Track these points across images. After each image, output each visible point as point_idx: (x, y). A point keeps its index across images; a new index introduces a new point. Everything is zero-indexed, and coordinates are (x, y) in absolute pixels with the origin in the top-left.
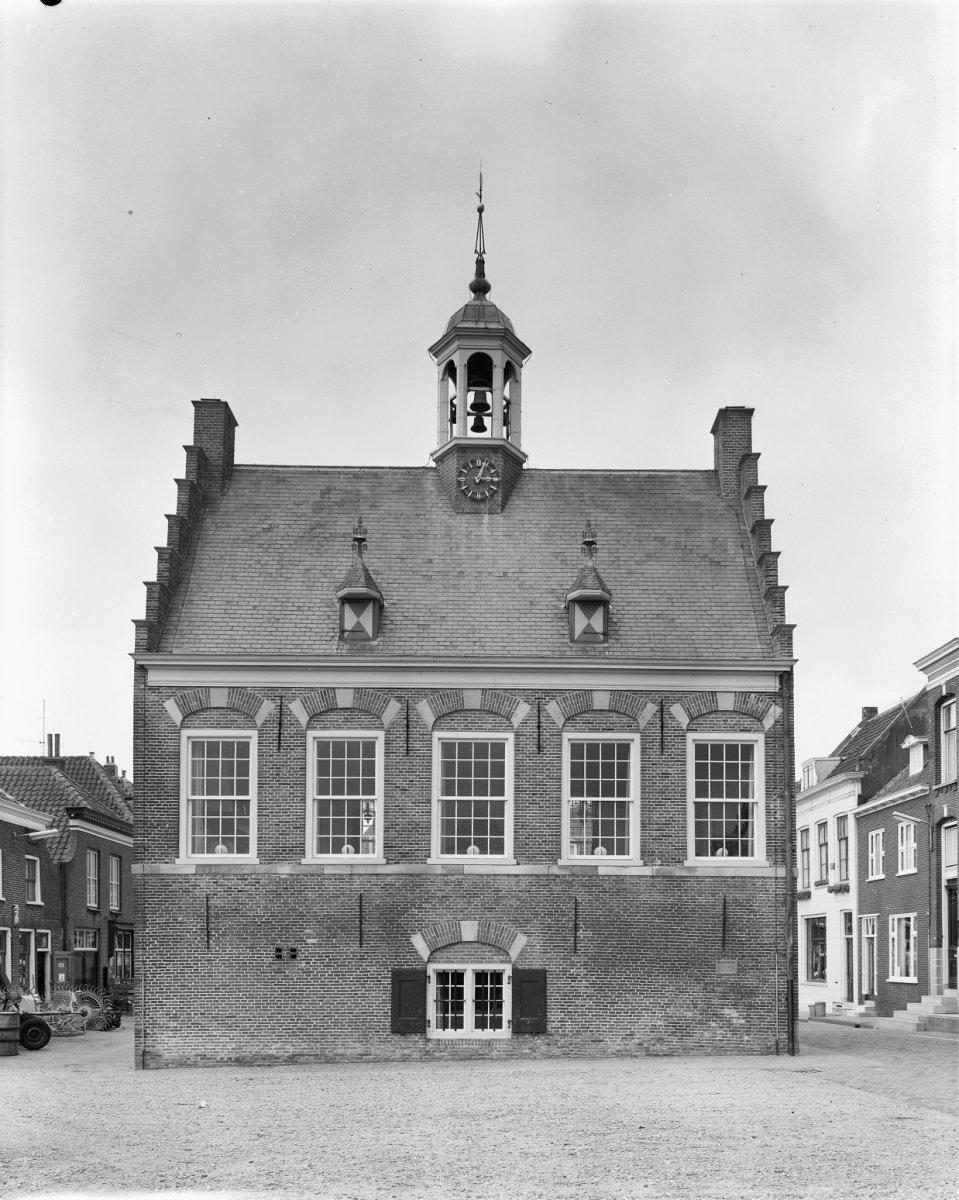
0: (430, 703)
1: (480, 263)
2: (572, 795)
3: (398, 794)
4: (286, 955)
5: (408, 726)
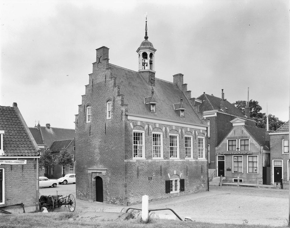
0: (169, 128)
1: (146, 33)
3: (165, 145)
4: (150, 179)
5: (166, 132)
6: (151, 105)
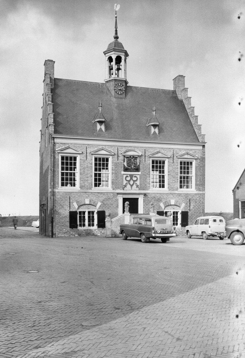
1: (116, 31)
2: (180, 174)
6: (152, 126)
